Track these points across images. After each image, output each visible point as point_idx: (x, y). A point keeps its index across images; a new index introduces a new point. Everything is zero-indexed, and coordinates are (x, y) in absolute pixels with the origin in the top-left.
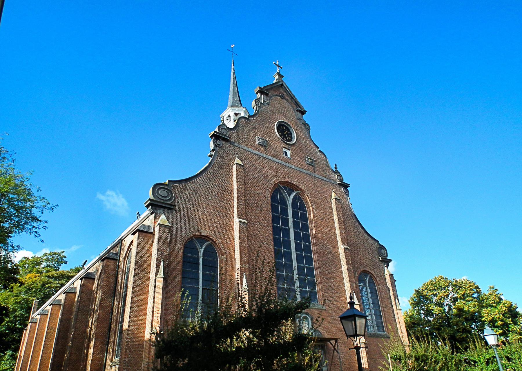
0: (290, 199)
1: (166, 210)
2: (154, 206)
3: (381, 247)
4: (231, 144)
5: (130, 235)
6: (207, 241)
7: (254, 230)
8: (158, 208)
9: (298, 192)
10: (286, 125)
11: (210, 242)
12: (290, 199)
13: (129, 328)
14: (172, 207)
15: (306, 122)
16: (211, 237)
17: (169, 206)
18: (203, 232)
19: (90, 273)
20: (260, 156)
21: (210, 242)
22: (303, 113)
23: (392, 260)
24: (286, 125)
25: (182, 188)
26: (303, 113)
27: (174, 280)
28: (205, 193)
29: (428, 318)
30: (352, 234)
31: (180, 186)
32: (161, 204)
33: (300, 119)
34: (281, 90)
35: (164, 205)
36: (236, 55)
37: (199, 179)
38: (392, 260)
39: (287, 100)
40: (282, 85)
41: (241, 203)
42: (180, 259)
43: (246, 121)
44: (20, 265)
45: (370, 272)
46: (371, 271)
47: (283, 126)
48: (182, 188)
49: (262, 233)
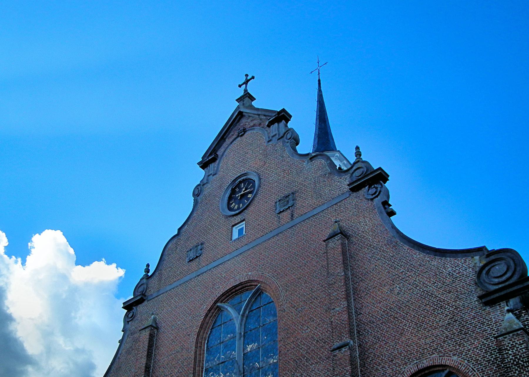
3: (493, 257)
30: (385, 289)
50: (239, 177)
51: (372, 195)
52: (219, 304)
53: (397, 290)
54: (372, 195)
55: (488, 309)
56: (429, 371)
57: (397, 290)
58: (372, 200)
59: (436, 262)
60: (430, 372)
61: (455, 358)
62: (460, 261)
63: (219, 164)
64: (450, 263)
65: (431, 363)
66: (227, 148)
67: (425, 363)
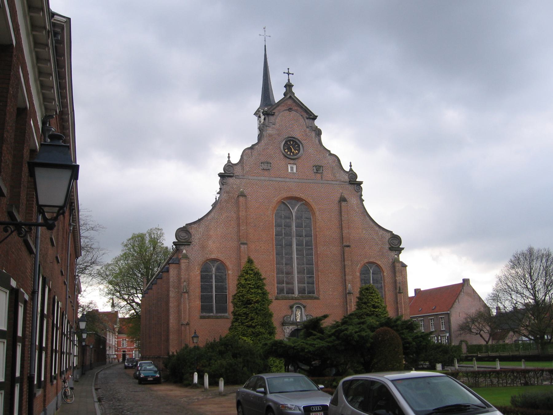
2: (139, 381)
4: (236, 178)
7: (255, 247)
8: (181, 246)
10: (294, 139)
11: (220, 262)
13: (133, 310)
14: (190, 244)
15: (318, 128)
16: (220, 259)
21: (220, 262)
22: (315, 118)
23: (404, 248)
24: (294, 139)
25: (196, 227)
26: (315, 118)
27: (195, 292)
28: (214, 227)
31: (195, 226)
36: (260, 35)
37: (209, 217)
38: (404, 248)
39: (296, 111)
41: (243, 229)
43: (250, 151)
44: (118, 299)
45: (376, 262)
47: (290, 141)
48: (196, 227)
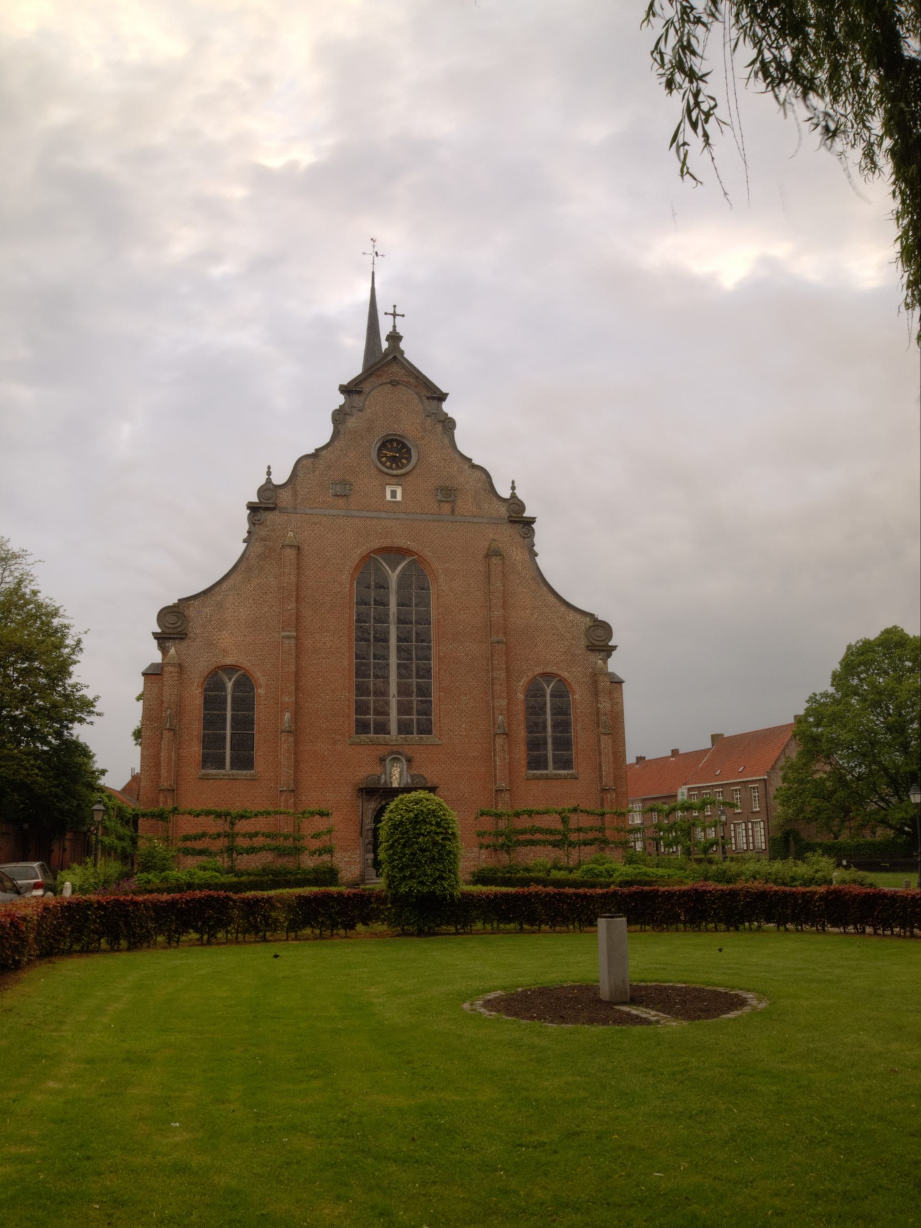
0: (393, 577)
1: (177, 641)
3: (597, 623)
5: (705, 125)
6: (239, 670)
9: (412, 558)
12: (393, 577)
17: (179, 636)
18: (229, 661)
19: (905, 246)
20: (334, 516)
29: (38, 745)
30: (528, 611)
32: (168, 636)
33: (433, 413)
34: (395, 368)
35: (172, 636)
40: (395, 358)
42: (197, 702)
46: (559, 673)
49: (328, 645)
50: (400, 436)
51: (172, 624)
52: (372, 555)
53: (536, 616)
54: (172, 624)
55: (589, 652)
56: (556, 891)
57: (536, 616)
58: (524, 538)
59: (563, 609)
60: (559, 894)
61: (566, 673)
62: (578, 616)
63: (365, 400)
64: (572, 615)
65: (552, 671)
66: (375, 388)
67: (548, 670)
